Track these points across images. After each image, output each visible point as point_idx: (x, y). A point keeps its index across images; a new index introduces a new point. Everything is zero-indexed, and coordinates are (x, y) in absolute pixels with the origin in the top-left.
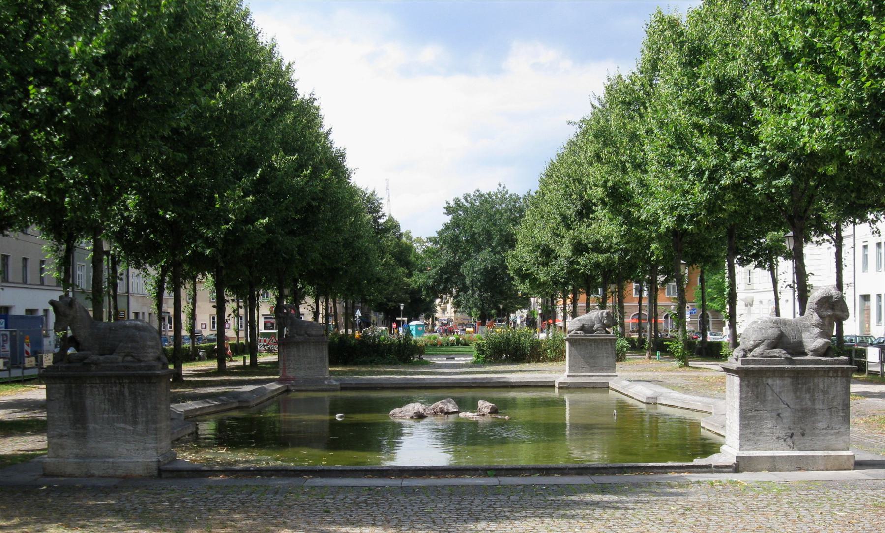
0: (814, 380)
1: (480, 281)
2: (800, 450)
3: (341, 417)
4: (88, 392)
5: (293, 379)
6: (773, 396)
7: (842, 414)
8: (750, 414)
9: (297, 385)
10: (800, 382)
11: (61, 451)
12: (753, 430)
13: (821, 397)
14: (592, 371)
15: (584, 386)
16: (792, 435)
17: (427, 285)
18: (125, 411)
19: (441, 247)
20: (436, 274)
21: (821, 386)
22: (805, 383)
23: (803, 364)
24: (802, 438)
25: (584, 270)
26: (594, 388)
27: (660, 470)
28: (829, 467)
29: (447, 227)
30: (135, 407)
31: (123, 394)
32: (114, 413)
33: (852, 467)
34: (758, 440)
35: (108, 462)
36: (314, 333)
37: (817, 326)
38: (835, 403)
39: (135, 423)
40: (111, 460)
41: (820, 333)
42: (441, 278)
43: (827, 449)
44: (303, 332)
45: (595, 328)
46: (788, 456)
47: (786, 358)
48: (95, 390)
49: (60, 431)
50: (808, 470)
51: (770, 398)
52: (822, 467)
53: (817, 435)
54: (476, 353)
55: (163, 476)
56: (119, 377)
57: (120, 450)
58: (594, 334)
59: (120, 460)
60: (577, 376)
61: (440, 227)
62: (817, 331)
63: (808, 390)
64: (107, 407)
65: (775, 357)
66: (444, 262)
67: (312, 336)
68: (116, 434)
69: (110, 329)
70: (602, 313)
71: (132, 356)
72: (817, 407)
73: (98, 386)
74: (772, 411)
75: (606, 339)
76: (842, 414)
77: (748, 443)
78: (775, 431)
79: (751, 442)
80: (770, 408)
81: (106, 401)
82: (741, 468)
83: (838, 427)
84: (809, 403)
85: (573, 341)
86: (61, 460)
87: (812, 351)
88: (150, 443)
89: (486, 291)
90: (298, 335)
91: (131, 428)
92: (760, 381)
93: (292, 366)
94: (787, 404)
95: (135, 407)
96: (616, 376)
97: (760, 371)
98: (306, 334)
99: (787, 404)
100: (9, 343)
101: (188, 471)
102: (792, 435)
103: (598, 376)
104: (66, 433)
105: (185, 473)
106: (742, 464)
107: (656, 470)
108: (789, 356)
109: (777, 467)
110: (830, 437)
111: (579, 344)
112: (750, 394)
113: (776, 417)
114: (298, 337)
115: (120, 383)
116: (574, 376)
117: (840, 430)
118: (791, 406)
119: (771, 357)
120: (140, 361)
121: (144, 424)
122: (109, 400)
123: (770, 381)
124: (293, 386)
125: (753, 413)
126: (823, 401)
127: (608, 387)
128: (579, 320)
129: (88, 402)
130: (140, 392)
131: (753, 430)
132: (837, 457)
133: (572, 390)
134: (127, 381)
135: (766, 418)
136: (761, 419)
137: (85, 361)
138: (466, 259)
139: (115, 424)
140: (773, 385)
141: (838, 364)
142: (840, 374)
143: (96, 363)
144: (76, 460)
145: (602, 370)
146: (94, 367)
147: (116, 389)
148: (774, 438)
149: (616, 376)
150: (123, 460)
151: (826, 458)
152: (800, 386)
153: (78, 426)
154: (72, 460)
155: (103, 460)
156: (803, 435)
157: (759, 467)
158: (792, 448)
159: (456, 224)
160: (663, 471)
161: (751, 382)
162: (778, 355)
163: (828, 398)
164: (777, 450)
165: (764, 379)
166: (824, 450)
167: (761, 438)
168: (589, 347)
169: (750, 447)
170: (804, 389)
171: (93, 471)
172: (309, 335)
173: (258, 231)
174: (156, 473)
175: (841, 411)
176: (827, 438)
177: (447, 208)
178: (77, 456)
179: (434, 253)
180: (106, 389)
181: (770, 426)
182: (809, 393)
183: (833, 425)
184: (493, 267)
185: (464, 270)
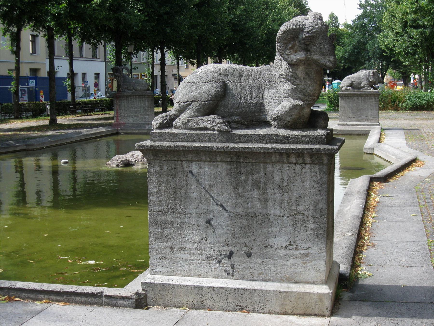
0: (265, 168)
2: (243, 278)
3: (65, 163)
5: (124, 124)
6: (199, 191)
7: (312, 226)
8: (164, 218)
9: (124, 129)
10: (243, 170)
12: (170, 244)
13: (278, 196)
15: (350, 133)
16: (231, 255)
17: (344, 57)
19: (355, 31)
21: (277, 178)
22: (252, 173)
23: (252, 142)
24: (247, 259)
25: (417, 43)
26: (358, 135)
27: (30, 295)
28: (288, 310)
29: (359, 18)
33: (328, 312)
34: (177, 258)
36: (139, 88)
37: (287, 78)
38: (301, 208)
41: (293, 90)
43: (289, 280)
45: (363, 84)
46: (222, 288)
47: (220, 131)
50: (254, 311)
51: (195, 194)
52: (277, 309)
53: (272, 257)
54: (328, 103)
61: (354, 18)
62: (287, 87)
63: (257, 185)
65: (206, 129)
70: (369, 73)
72: (272, 212)
74: (199, 214)
75: (371, 95)
76: (312, 226)
77: (162, 262)
78: (203, 247)
79: (167, 262)
80: (194, 211)
82: (150, 301)
83: (305, 246)
84: (258, 205)
87: (274, 120)
90: (129, 90)
92: (179, 168)
93: (122, 114)
94: (222, 205)
97: (186, 151)
99: (222, 205)
100: (27, 95)
102: (231, 255)
103: (363, 125)
106: (151, 295)
107: (24, 295)
108: (225, 128)
109: (205, 303)
110: (292, 261)
111: (348, 98)
112: (163, 188)
113: (204, 225)
116: (343, 125)
117: (310, 251)
118: (229, 209)
119: (201, 129)
123: (194, 168)
124: (121, 129)
125: (169, 217)
126: (281, 203)
128: (349, 78)
131: (170, 244)
132: (301, 295)
135: (190, 226)
136: (182, 227)
140: (199, 174)
141: (308, 143)
142: (308, 160)
145: (367, 120)
148: (204, 257)
151: (283, 295)
152: (243, 177)
156: (249, 255)
157: (177, 301)
158: (231, 275)
159: (364, 15)
160: (33, 296)
161: (165, 168)
162: (209, 126)
163: (289, 198)
164: (207, 277)
165: (185, 164)
166: (283, 281)
167: (182, 255)
168: (356, 100)
169: (166, 270)
170: (249, 182)
172: (136, 90)
173: (94, 10)
175: (312, 220)
176: (288, 263)
177: (359, 5)
181: (195, 238)
182: (258, 188)
183: (298, 242)
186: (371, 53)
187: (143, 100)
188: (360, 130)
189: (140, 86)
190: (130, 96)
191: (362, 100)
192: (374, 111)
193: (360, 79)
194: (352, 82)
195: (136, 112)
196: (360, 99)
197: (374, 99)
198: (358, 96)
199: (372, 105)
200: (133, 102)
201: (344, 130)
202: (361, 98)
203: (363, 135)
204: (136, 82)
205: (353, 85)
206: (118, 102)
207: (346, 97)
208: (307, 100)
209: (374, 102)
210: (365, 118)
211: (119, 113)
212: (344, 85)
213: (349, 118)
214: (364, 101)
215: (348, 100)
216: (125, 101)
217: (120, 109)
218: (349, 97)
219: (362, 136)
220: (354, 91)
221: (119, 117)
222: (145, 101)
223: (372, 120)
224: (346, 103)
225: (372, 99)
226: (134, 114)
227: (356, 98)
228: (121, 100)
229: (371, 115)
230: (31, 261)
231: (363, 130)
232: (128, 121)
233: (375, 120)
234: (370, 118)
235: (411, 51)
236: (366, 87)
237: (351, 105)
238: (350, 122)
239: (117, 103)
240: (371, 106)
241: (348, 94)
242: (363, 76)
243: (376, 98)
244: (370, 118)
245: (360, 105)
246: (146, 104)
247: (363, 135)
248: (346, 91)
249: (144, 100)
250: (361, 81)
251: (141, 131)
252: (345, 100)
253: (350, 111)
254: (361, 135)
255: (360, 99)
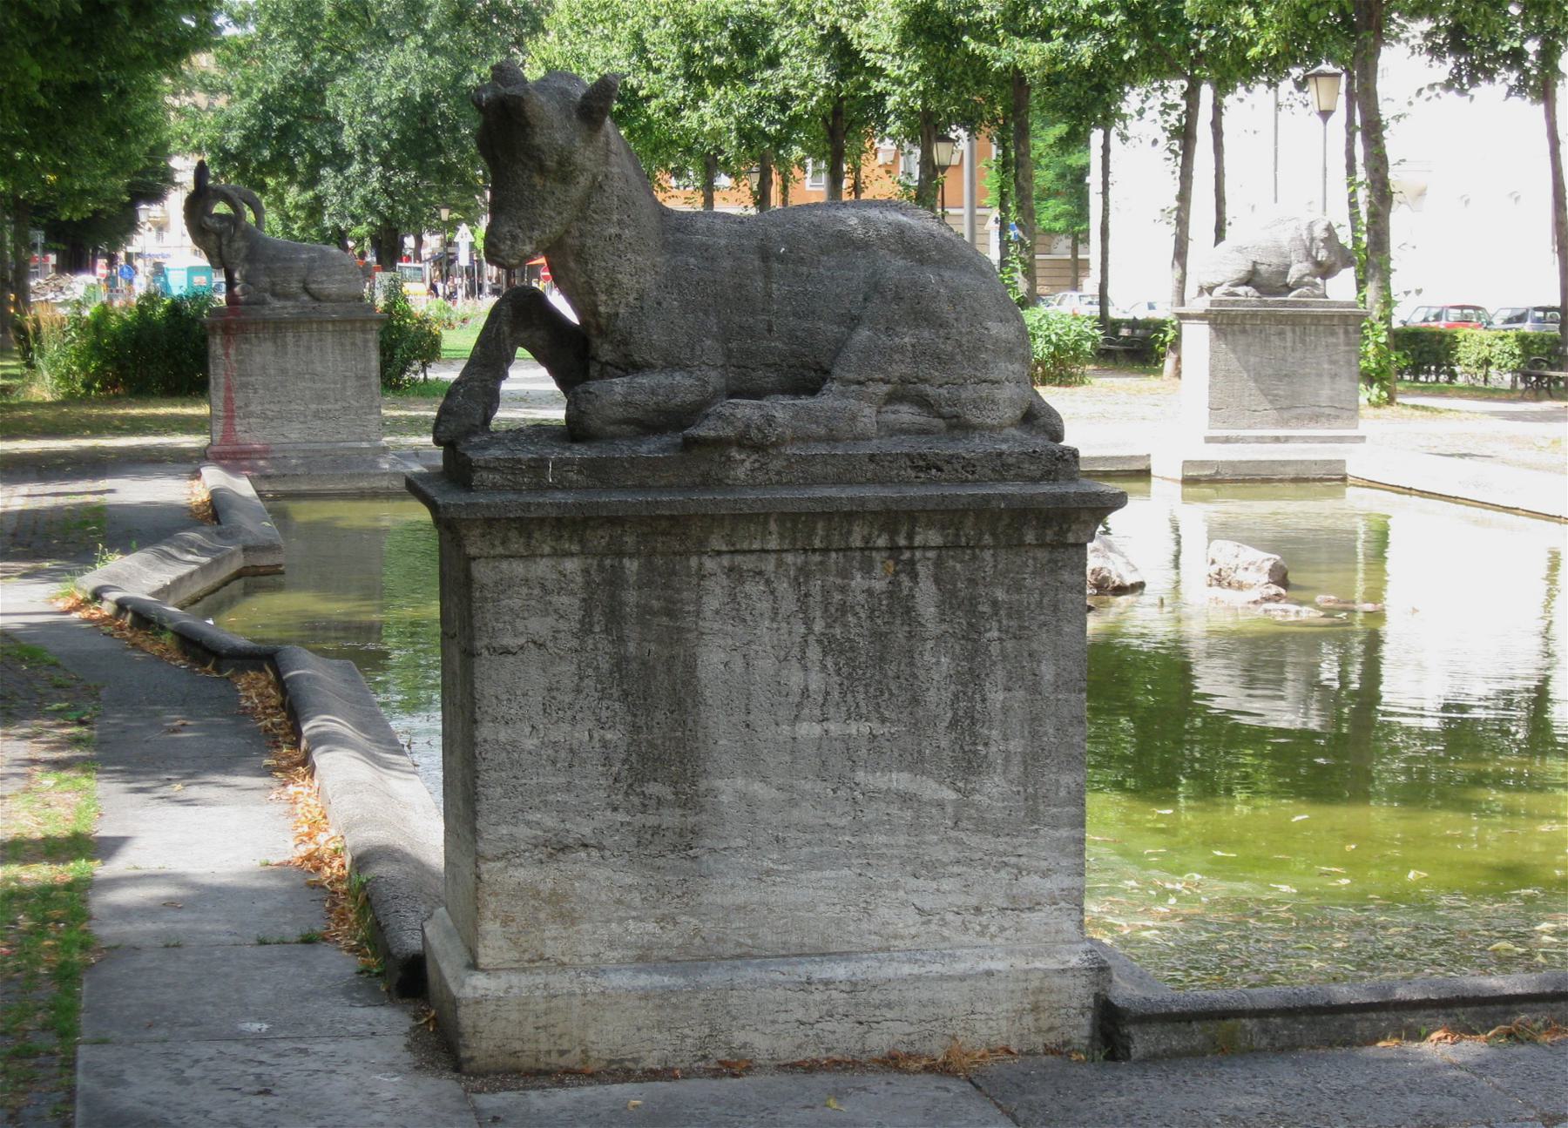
1: (387, 137)
4: (712, 603)
5: (264, 453)
11: (553, 930)
14: (1284, 423)
15: (1265, 473)
17: (222, 149)
18: (915, 701)
20: (252, 113)
26: (1296, 480)
30: (970, 678)
31: (905, 609)
32: (854, 715)
35: (827, 983)
36: (332, 288)
39: (969, 764)
40: (840, 971)
42: (266, 126)
44: (295, 286)
45: (1292, 277)
48: (753, 588)
49: (550, 821)
55: (1138, 1048)
56: (893, 518)
57: (884, 912)
58: (1291, 297)
59: (889, 971)
60: (1237, 440)
64: (816, 681)
66: (276, 77)
67: (328, 298)
68: (861, 828)
69: (765, 255)
71: (923, 402)
73: (769, 565)
81: (814, 653)
85: (1223, 322)
86: (561, 982)
88: (1045, 874)
89: (403, 168)
91: (950, 795)
95: (970, 678)
96: (1362, 439)
98: (306, 290)
101: (1261, 1014)
103: (1305, 439)
104: (586, 829)
105: (1248, 1023)
111: (1244, 331)
114: (277, 304)
115: (894, 549)
116: (1227, 440)
120: (959, 426)
121: (1016, 770)
122: (828, 645)
127: (1344, 479)
129: (712, 659)
130: (1000, 595)
133: (1227, 489)
134: (934, 538)
137: (704, 431)
138: (342, 70)
139: (860, 776)
143: (756, 443)
144: (643, 980)
145: (1315, 418)
146: (743, 465)
147: (866, 584)
149: (1362, 439)
150: (906, 969)
153: (653, 788)
154: (620, 980)
155: (804, 969)
168: (1275, 340)
171: (739, 1037)
172: (315, 297)
174: (1080, 1029)
178: (644, 959)
179: (240, 51)
180: (816, 586)
184: (426, 96)
185: (342, 99)
186: (348, 139)
187: (353, 344)
188: (1302, 462)
189: (338, 277)
190: (296, 323)
191: (1297, 339)
192: (1343, 384)
193: (1282, 255)
194: (1255, 263)
195: (321, 398)
196: (1289, 335)
197: (1342, 336)
198: (1280, 323)
199: (1335, 357)
200: (309, 349)
201: (1241, 462)
202: (1294, 332)
203: (1314, 480)
204: (313, 260)
205: (1257, 279)
206: (232, 351)
207: (1236, 327)
208: (12, 408)
209: (1342, 348)
210: (1308, 411)
211: (238, 403)
212: (1220, 280)
213: (1247, 413)
214: (1303, 342)
215: (1242, 340)
216: (268, 346)
217: (244, 386)
218: (1248, 327)
219: (1311, 484)
220: (1266, 304)
221: (237, 421)
222: (365, 346)
223: (1337, 417)
224: (1234, 351)
225: (1333, 334)
226: (313, 407)
227: (1273, 329)
228: (247, 340)
229: (1331, 398)
230: (256, 1026)
231: (1316, 463)
232: (281, 440)
233: (1348, 418)
234: (1327, 411)
235: (772, 130)
236: (1307, 284)
237: (1252, 359)
238: (1249, 427)
239: (227, 355)
240: (1333, 362)
241: (1244, 315)
242: (1293, 240)
243: (1351, 329)
244: (1327, 411)
245: (1290, 360)
246: (368, 361)
247: (1314, 480)
248: (1234, 303)
249: (359, 342)
250: (1287, 261)
251: (364, 484)
252: (1229, 337)
253: (1252, 384)
254: (1307, 480)
255: (1289, 335)
